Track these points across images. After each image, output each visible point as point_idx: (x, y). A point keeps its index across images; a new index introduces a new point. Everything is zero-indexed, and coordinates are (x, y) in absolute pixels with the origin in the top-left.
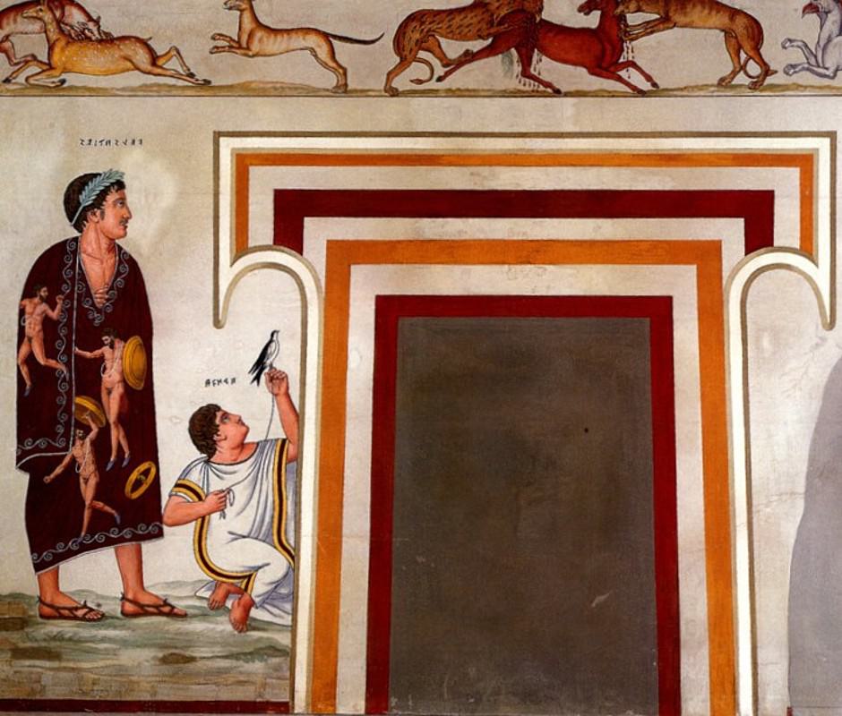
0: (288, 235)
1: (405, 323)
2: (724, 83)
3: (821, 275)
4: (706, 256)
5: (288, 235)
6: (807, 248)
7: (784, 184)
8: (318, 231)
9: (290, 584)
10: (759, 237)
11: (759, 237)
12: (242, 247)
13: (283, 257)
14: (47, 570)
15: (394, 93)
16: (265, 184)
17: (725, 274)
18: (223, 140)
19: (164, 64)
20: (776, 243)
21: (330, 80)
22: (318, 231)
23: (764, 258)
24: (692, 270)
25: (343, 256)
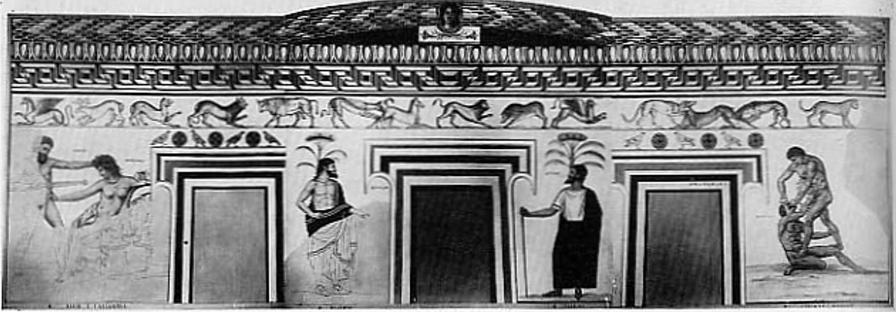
0: (385, 168)
1: (418, 193)
2: (772, 126)
3: (532, 178)
4: (501, 174)
5: (385, 168)
6: (528, 172)
7: (379, 153)
8: (394, 167)
9: (482, 287)
10: (516, 169)
14: (624, 288)
15: (440, 127)
19: (752, 121)
21: (541, 123)
22: (394, 167)
24: (728, 183)
25: (401, 173)
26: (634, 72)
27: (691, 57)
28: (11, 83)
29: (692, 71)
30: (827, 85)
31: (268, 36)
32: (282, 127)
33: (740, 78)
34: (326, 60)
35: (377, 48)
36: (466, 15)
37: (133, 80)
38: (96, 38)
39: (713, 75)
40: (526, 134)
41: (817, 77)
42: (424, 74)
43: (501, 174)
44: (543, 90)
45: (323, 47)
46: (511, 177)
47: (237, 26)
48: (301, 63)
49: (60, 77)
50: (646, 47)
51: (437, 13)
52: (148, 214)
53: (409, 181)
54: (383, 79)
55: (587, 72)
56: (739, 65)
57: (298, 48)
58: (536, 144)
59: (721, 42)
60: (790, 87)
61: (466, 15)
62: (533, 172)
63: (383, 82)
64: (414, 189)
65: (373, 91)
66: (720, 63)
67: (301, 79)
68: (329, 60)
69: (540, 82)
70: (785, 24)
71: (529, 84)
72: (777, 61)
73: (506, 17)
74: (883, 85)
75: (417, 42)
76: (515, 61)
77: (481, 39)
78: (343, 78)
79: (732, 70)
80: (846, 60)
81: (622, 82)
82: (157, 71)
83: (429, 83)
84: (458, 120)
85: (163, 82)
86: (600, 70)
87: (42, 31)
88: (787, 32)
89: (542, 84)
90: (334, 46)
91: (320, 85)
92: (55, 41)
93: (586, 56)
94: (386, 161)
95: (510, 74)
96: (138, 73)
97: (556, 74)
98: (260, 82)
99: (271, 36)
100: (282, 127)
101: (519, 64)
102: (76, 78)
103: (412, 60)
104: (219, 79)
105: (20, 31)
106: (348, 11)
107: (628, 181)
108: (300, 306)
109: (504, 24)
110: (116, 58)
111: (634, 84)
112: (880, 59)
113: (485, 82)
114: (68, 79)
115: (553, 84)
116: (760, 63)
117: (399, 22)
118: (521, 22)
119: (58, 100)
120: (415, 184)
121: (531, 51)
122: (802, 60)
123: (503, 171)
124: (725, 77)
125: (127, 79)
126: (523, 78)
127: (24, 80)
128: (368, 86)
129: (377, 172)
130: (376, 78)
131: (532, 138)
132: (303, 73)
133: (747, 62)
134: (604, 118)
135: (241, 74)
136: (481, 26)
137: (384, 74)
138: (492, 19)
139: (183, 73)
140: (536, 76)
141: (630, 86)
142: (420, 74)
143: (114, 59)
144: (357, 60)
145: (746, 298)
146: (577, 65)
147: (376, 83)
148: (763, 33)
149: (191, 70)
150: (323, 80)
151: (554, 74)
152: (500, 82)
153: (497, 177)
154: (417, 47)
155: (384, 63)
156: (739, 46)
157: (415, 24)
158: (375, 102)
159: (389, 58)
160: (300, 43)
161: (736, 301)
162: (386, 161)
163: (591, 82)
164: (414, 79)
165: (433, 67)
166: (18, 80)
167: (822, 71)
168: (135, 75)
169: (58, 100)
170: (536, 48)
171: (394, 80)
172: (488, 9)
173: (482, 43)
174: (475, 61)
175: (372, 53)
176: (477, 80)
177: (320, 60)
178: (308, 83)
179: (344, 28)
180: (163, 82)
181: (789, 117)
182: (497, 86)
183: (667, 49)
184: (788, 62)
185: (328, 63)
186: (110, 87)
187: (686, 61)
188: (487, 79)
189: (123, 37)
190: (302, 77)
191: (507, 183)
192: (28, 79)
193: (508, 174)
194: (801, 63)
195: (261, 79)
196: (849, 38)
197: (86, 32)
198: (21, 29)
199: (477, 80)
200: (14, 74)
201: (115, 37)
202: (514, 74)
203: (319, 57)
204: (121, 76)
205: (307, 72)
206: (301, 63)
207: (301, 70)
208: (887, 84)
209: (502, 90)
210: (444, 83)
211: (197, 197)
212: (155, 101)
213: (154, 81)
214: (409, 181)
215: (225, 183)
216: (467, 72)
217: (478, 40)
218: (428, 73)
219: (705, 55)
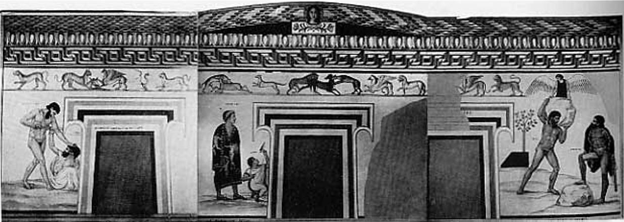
0: (268, 123)
3: (511, 131)
4: (349, 128)
5: (268, 123)
7: (364, 113)
10: (499, 125)
11: (499, 125)
13: (266, 127)
16: (263, 112)
17: (353, 130)
18: (261, 110)
22: (274, 122)
25: (278, 127)
27: (349, 44)
28: (3, 61)
29: (512, 55)
30: (380, 65)
31: (264, 18)
32: (48, 90)
33: (447, 56)
34: (187, 44)
35: (233, 35)
36: (325, 15)
37: (33, 58)
39: (443, 58)
40: (134, 94)
41: (345, 59)
42: (238, 54)
44: (435, 68)
45: (263, 36)
46: (356, 129)
47: (211, 20)
48: (208, 46)
50: (451, 38)
51: (304, 13)
53: (284, 133)
54: (295, 59)
56: (603, 50)
57: (205, 36)
58: (374, 107)
59: (503, 34)
60: (410, 67)
61: (325, 15)
63: (238, 60)
64: (287, 138)
65: (15, 64)
66: (503, 50)
67: (208, 58)
68: (113, 43)
69: (573, 61)
70: (550, 23)
71: (510, 63)
72: (543, 48)
73: (353, 16)
74: (617, 62)
75: (291, 33)
76: (330, 46)
77: (336, 31)
78: (239, 58)
79: (512, 55)
80: (554, 47)
81: (547, 62)
82: (164, 52)
83: (270, 62)
84: (75, 85)
86: (334, 53)
87: (228, 19)
88: (452, 28)
89: (436, 61)
90: (261, 35)
91: (222, 62)
93: (515, 43)
94: (268, 118)
95: (411, 56)
96: (151, 54)
97: (613, 55)
98: (10, 59)
100: (48, 90)
101: (333, 48)
102: (35, 53)
103: (170, 43)
105: (212, 22)
106: (241, 11)
107: (273, 127)
109: (352, 21)
110: (203, 44)
111: (500, 64)
112: (500, 46)
113: (563, 62)
115: (413, 63)
116: (474, 49)
117: (277, 19)
118: (364, 20)
119: (479, 77)
120: (484, 137)
121: (399, 40)
122: (531, 48)
123: (492, 127)
124: (479, 59)
125: (171, 58)
126: (532, 58)
128: (541, 66)
131: (63, 100)
133: (522, 49)
134: (254, 83)
136: (336, 22)
137: (267, 55)
138: (368, 20)
139: (69, 52)
140: (430, 59)
141: (384, 65)
142: (236, 54)
143: (252, 46)
144: (277, 45)
145: (500, 213)
146: (403, 50)
150: (224, 59)
151: (359, 56)
152: (461, 62)
153: (346, 130)
154: (291, 36)
155: (237, 47)
156: (468, 37)
157: (289, 21)
158: (302, 77)
159: (280, 44)
160: (207, 33)
161: (493, 216)
162: (268, 118)
163: (441, 62)
165: (302, 50)
166: (94, 59)
167: (574, 55)
168: (149, 54)
169: (479, 77)
170: (288, 36)
171: (274, 60)
172: (341, 10)
173: (337, 34)
174: (610, 46)
175: (208, 39)
176: (360, 61)
177: (222, 45)
178: (212, 61)
179: (237, 23)
180: (168, 59)
181: (126, 83)
182: (543, 65)
183: (332, 38)
184: (170, 45)
185: (287, 48)
186: (275, 62)
187: (518, 48)
188: (453, 61)
189: (31, 27)
190: (209, 57)
191: (493, 133)
192: (43, 58)
193: (354, 127)
194: (504, 49)
198: (212, 21)
199: (388, 61)
200: (6, 54)
202: (386, 56)
203: (280, 44)
205: (299, 55)
206: (208, 46)
207: (295, 53)
208: (620, 61)
210: (310, 62)
211: (103, 144)
212: (81, 72)
213: (79, 58)
214: (284, 133)
216: (325, 54)
217: (334, 32)
218: (212, 53)
219: (493, 44)
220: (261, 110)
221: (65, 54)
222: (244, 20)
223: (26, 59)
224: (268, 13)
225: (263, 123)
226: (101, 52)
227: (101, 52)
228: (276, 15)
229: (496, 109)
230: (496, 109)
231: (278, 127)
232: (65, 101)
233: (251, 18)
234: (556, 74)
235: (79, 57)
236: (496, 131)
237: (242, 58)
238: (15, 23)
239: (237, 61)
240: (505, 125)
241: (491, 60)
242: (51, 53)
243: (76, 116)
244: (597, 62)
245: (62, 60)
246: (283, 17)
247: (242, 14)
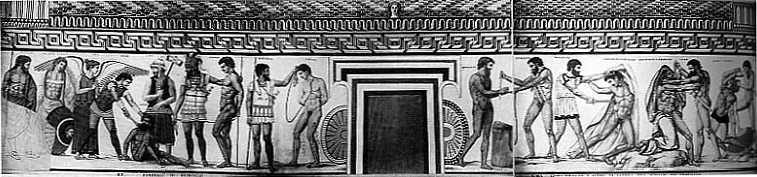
4: (434, 81)
5: (344, 78)
6: (455, 81)
10: (446, 78)
11: (446, 78)
12: (335, 80)
13: (343, 82)
20: (450, 79)
22: (350, 77)
23: (447, 82)
25: (355, 82)
26: (540, 37)
31: (592, 11)
37: (121, 45)
38: (486, 13)
39: (718, 40)
42: (376, 40)
43: (434, 81)
49: (249, 44)
52: (460, 97)
55: (714, 37)
62: (458, 80)
63: (284, 46)
67: (375, 45)
71: (552, 46)
78: (376, 43)
85: (174, 46)
87: (499, 8)
92: (481, 16)
99: (616, 14)
104: (187, 44)
108: (5, 111)
114: (255, 46)
127: (221, 47)
128: (675, 47)
129: (339, 81)
130: (385, 43)
132: (376, 40)
135: (204, 41)
137: (345, 40)
147: (324, 43)
148: (170, 8)
149: (258, 38)
163: (538, 44)
164: (734, 42)
180: (205, 46)
192: (163, 45)
195: (189, 44)
196: (72, 10)
197: (637, 11)
198: (619, 8)
201: (501, 12)
204: (143, 42)
209: (450, 48)
215: (375, 87)
218: (379, 39)
220: (453, 64)
221: (79, 42)
222: (487, 11)
223: (82, 44)
224: (487, 6)
225: (340, 79)
226: (193, 39)
227: (193, 39)
228: (468, 9)
229: (335, 71)
230: (335, 71)
231: (355, 82)
232: (335, 67)
233: (496, 10)
234: (221, 57)
235: (77, 43)
236: (441, 84)
237: (349, 43)
238: (721, 9)
239: (344, 47)
240: (453, 79)
241: (653, 42)
242: (338, 40)
243: (339, 77)
244: (429, 46)
245: (30, 44)
246: (158, 8)
247: (486, 4)
